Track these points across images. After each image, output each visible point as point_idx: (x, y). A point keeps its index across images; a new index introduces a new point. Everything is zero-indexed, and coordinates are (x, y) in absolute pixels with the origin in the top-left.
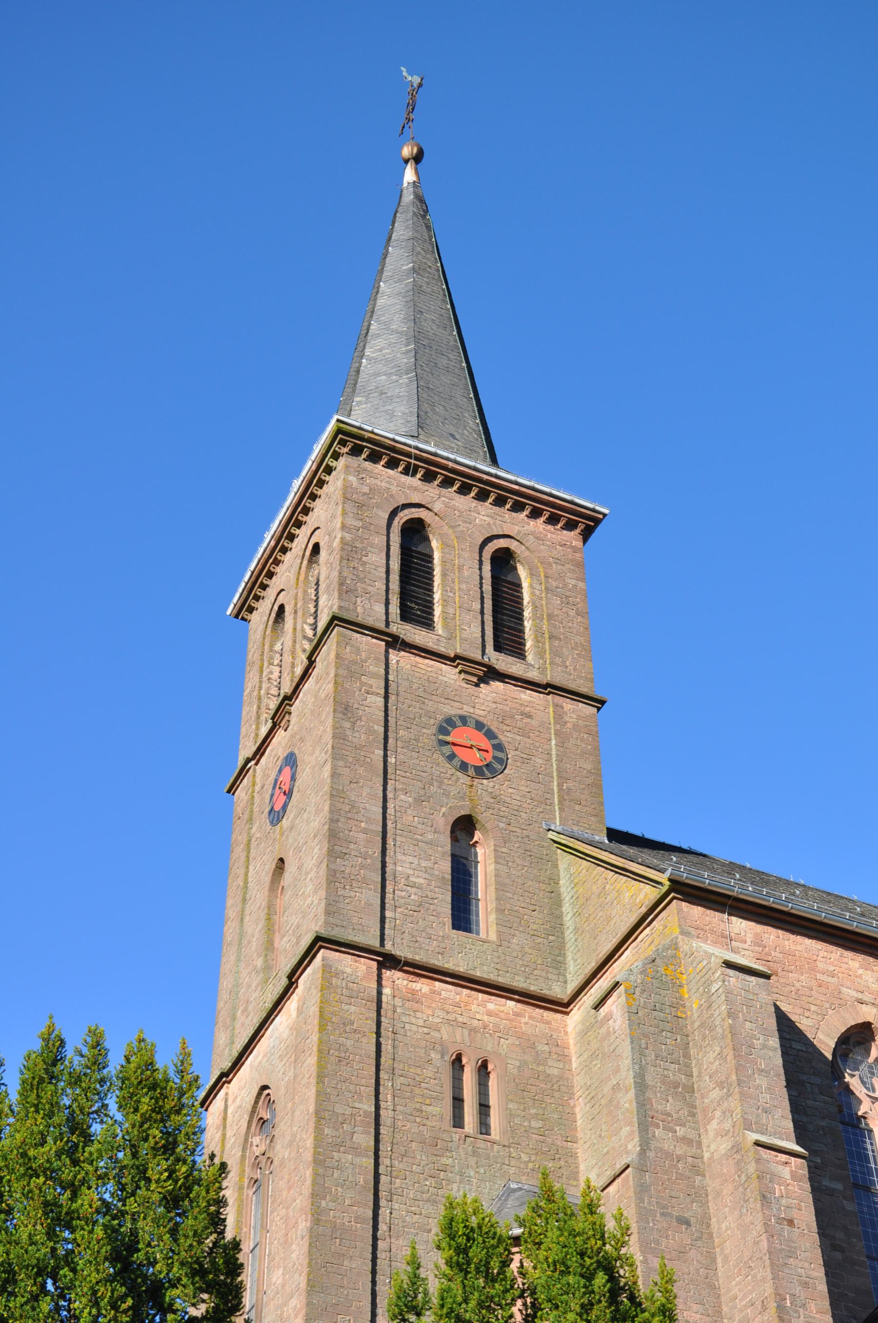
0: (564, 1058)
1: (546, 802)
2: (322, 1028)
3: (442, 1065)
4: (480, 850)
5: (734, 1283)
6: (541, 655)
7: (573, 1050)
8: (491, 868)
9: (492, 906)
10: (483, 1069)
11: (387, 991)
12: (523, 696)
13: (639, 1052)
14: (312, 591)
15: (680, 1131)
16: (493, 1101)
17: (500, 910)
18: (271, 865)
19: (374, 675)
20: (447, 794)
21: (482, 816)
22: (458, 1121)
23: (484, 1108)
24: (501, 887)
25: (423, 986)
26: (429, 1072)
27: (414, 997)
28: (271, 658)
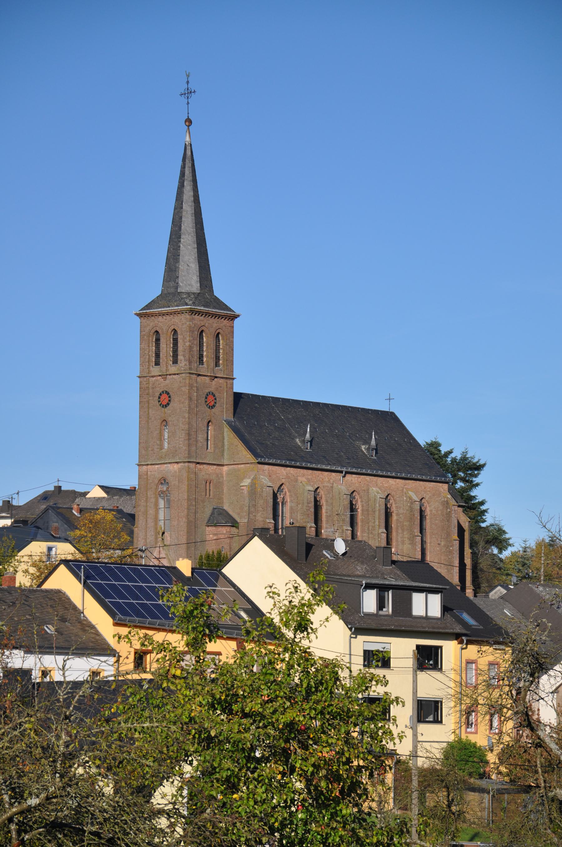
0: (223, 477)
1: (223, 412)
7: (224, 475)
25: (202, 467)
27: (200, 470)
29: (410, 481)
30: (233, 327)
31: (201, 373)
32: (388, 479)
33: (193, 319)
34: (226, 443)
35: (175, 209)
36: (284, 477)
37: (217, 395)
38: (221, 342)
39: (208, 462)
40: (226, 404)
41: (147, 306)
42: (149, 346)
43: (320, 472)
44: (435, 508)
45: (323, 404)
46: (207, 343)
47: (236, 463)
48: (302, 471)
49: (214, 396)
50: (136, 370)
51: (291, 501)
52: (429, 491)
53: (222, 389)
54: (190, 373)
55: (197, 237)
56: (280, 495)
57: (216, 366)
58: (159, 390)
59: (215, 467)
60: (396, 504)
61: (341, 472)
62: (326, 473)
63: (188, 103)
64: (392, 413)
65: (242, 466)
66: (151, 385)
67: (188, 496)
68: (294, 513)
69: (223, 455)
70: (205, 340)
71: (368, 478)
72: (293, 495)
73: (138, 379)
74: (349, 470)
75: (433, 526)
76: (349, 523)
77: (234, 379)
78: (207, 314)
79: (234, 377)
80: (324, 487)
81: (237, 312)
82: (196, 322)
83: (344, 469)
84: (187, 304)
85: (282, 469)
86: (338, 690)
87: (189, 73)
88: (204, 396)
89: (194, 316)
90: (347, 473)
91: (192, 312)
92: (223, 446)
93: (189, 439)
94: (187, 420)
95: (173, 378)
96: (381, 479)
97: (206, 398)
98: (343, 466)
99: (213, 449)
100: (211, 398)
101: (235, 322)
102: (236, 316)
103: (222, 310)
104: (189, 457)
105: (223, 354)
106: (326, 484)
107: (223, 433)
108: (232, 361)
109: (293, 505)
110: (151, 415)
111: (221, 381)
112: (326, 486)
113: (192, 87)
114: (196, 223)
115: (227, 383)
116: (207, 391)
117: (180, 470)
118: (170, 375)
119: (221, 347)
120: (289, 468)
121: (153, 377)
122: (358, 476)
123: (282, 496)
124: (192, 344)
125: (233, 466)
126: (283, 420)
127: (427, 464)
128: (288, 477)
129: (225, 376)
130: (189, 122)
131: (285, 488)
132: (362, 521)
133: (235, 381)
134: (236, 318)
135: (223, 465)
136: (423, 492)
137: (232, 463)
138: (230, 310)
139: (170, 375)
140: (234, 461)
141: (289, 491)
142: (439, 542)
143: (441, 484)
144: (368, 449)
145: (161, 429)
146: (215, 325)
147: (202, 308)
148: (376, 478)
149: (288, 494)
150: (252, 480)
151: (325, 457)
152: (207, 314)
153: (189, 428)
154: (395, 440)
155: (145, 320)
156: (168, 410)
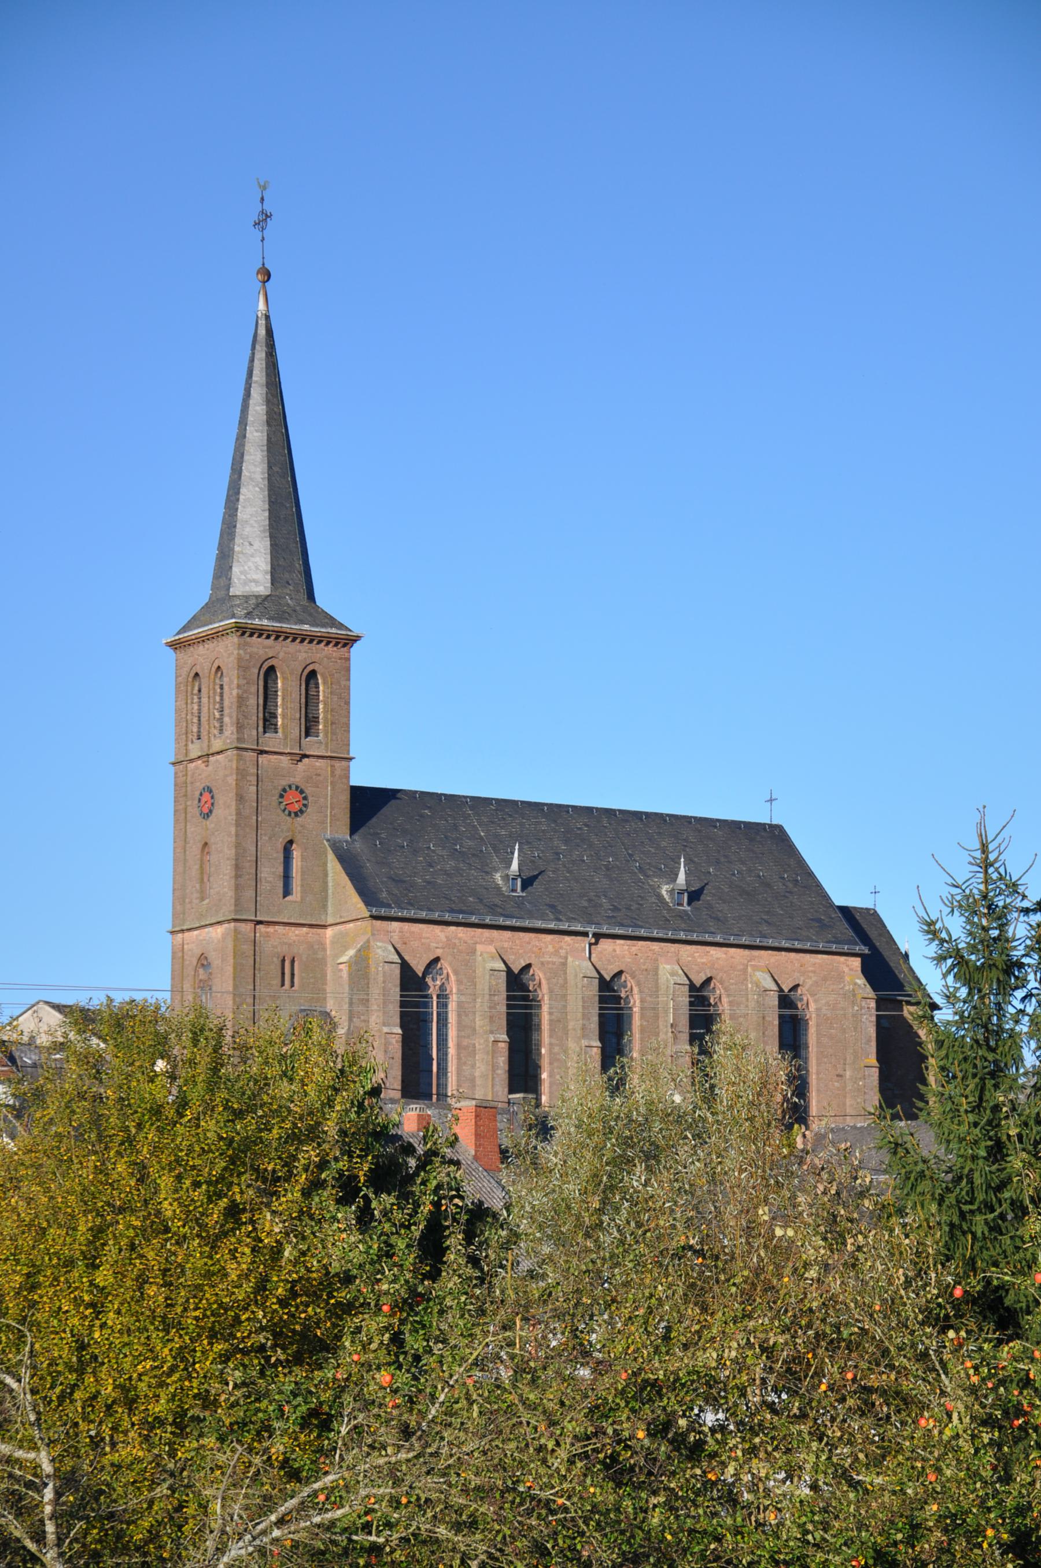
0: (324, 950)
1: (324, 822)
2: (234, 957)
3: (277, 961)
4: (295, 853)
5: (267, 1224)
6: (326, 735)
7: (328, 946)
8: (299, 864)
9: (299, 883)
10: (293, 961)
11: (258, 935)
12: (317, 764)
13: (351, 989)
14: (218, 699)
15: (362, 1017)
16: (296, 972)
17: (302, 886)
18: (200, 845)
19: (252, 775)
20: (282, 831)
21: (295, 840)
22: (283, 985)
23: (293, 975)
24: (303, 873)
25: (271, 929)
26: (272, 967)
27: (267, 935)
28: (193, 699)
29: (762, 952)
30: (348, 659)
31: (266, 749)
32: (708, 948)
33: (246, 644)
34: (330, 884)
35: (237, 439)
36: (440, 945)
37: (308, 791)
38: (321, 688)
39: (285, 920)
40: (332, 809)
41: (184, 627)
42: (187, 703)
43: (532, 935)
44: (827, 1004)
45: (523, 802)
46: (284, 690)
47: (343, 920)
48: (486, 933)
49: (302, 792)
50: (169, 752)
51: (460, 992)
52: (814, 972)
53: (321, 778)
54: (238, 748)
55: (269, 490)
56: (434, 980)
57: (307, 734)
58: (199, 786)
59: (305, 929)
60: (728, 996)
61: (585, 934)
62: (549, 938)
63: (263, 240)
64: (780, 828)
65: (351, 925)
66: (189, 778)
67: (235, 987)
68: (467, 1015)
69: (324, 907)
70: (280, 685)
71: (656, 946)
72: (465, 981)
73: (172, 768)
74: (605, 929)
75: (825, 1040)
76: (597, 1033)
77: (351, 759)
78: (278, 635)
79: (352, 755)
80: (542, 963)
81: (356, 631)
82: (255, 650)
83: (591, 929)
84: (233, 616)
85: (437, 929)
86: (832, 1366)
87: (266, 182)
88: (277, 793)
89: (249, 639)
90: (598, 936)
91: (242, 630)
92: (325, 888)
93: (237, 876)
94: (234, 839)
95: (217, 761)
96: (688, 947)
97: (281, 796)
98: (590, 923)
99: (299, 895)
100: (292, 797)
101: (352, 650)
102: (355, 639)
103: (317, 625)
104: (236, 912)
105: (325, 712)
106: (547, 958)
107: (325, 864)
108: (347, 725)
109: (463, 999)
110: (189, 835)
111: (320, 763)
112: (548, 963)
113: (268, 207)
114: (269, 462)
115: (332, 766)
116: (284, 783)
117: (224, 936)
118: (213, 754)
119: (321, 698)
120: (453, 928)
121: (191, 761)
122: (629, 942)
123: (438, 983)
124: (245, 691)
125: (339, 927)
126: (481, 838)
127: (819, 920)
128: (449, 944)
129: (329, 754)
130: (266, 275)
131: (445, 965)
132: (642, 1030)
133: (352, 763)
134: (355, 641)
135: (324, 927)
136: (797, 974)
137: (338, 921)
138: (341, 626)
139: (213, 754)
140: (341, 917)
141: (456, 973)
142: (840, 1071)
143: (843, 959)
144: (671, 892)
145: (202, 860)
146: (302, 656)
147: (265, 622)
148: (676, 945)
149: (452, 977)
150: (359, 950)
151: (552, 907)
152: (278, 635)
153: (237, 854)
154: (759, 876)
155: (181, 655)
156: (210, 823)
